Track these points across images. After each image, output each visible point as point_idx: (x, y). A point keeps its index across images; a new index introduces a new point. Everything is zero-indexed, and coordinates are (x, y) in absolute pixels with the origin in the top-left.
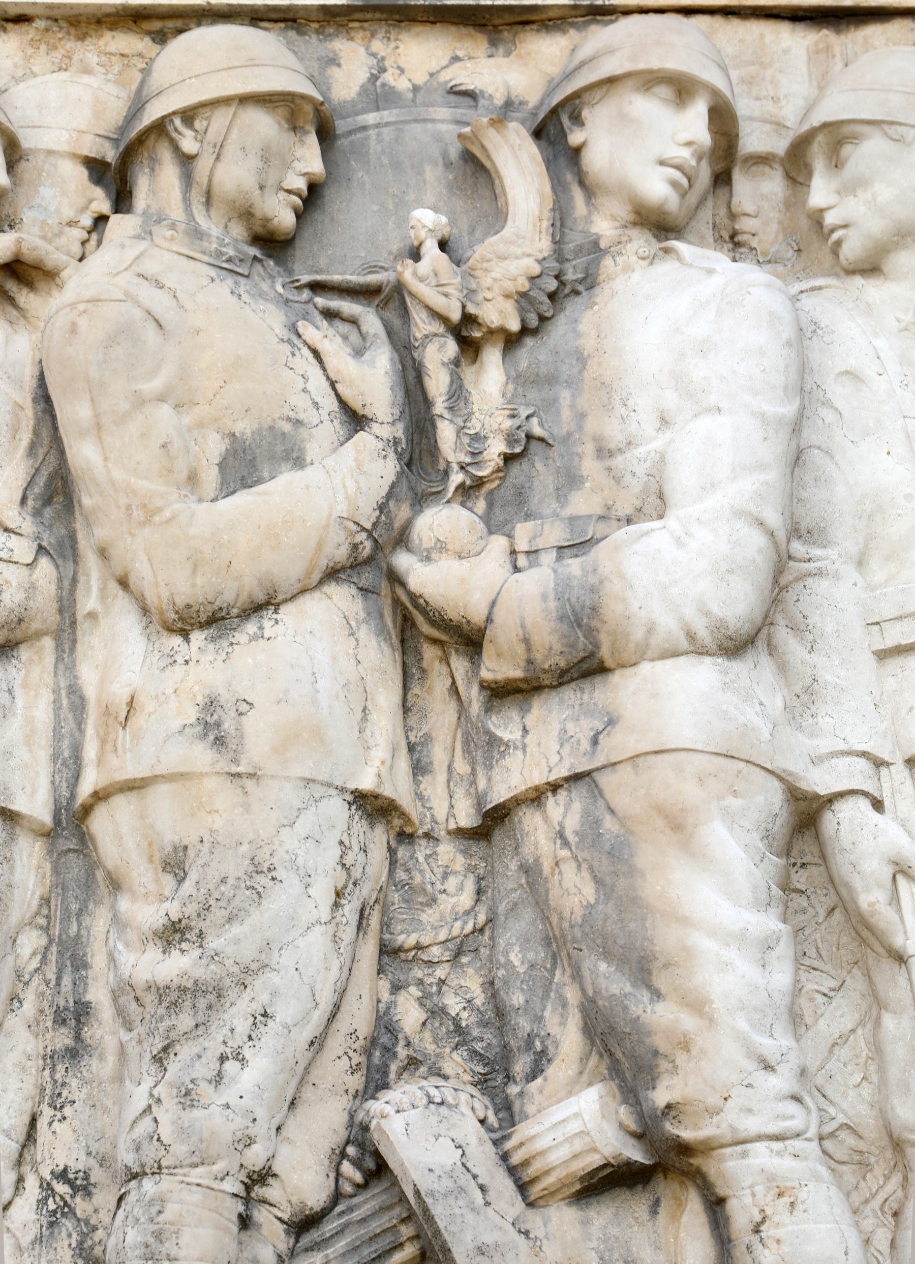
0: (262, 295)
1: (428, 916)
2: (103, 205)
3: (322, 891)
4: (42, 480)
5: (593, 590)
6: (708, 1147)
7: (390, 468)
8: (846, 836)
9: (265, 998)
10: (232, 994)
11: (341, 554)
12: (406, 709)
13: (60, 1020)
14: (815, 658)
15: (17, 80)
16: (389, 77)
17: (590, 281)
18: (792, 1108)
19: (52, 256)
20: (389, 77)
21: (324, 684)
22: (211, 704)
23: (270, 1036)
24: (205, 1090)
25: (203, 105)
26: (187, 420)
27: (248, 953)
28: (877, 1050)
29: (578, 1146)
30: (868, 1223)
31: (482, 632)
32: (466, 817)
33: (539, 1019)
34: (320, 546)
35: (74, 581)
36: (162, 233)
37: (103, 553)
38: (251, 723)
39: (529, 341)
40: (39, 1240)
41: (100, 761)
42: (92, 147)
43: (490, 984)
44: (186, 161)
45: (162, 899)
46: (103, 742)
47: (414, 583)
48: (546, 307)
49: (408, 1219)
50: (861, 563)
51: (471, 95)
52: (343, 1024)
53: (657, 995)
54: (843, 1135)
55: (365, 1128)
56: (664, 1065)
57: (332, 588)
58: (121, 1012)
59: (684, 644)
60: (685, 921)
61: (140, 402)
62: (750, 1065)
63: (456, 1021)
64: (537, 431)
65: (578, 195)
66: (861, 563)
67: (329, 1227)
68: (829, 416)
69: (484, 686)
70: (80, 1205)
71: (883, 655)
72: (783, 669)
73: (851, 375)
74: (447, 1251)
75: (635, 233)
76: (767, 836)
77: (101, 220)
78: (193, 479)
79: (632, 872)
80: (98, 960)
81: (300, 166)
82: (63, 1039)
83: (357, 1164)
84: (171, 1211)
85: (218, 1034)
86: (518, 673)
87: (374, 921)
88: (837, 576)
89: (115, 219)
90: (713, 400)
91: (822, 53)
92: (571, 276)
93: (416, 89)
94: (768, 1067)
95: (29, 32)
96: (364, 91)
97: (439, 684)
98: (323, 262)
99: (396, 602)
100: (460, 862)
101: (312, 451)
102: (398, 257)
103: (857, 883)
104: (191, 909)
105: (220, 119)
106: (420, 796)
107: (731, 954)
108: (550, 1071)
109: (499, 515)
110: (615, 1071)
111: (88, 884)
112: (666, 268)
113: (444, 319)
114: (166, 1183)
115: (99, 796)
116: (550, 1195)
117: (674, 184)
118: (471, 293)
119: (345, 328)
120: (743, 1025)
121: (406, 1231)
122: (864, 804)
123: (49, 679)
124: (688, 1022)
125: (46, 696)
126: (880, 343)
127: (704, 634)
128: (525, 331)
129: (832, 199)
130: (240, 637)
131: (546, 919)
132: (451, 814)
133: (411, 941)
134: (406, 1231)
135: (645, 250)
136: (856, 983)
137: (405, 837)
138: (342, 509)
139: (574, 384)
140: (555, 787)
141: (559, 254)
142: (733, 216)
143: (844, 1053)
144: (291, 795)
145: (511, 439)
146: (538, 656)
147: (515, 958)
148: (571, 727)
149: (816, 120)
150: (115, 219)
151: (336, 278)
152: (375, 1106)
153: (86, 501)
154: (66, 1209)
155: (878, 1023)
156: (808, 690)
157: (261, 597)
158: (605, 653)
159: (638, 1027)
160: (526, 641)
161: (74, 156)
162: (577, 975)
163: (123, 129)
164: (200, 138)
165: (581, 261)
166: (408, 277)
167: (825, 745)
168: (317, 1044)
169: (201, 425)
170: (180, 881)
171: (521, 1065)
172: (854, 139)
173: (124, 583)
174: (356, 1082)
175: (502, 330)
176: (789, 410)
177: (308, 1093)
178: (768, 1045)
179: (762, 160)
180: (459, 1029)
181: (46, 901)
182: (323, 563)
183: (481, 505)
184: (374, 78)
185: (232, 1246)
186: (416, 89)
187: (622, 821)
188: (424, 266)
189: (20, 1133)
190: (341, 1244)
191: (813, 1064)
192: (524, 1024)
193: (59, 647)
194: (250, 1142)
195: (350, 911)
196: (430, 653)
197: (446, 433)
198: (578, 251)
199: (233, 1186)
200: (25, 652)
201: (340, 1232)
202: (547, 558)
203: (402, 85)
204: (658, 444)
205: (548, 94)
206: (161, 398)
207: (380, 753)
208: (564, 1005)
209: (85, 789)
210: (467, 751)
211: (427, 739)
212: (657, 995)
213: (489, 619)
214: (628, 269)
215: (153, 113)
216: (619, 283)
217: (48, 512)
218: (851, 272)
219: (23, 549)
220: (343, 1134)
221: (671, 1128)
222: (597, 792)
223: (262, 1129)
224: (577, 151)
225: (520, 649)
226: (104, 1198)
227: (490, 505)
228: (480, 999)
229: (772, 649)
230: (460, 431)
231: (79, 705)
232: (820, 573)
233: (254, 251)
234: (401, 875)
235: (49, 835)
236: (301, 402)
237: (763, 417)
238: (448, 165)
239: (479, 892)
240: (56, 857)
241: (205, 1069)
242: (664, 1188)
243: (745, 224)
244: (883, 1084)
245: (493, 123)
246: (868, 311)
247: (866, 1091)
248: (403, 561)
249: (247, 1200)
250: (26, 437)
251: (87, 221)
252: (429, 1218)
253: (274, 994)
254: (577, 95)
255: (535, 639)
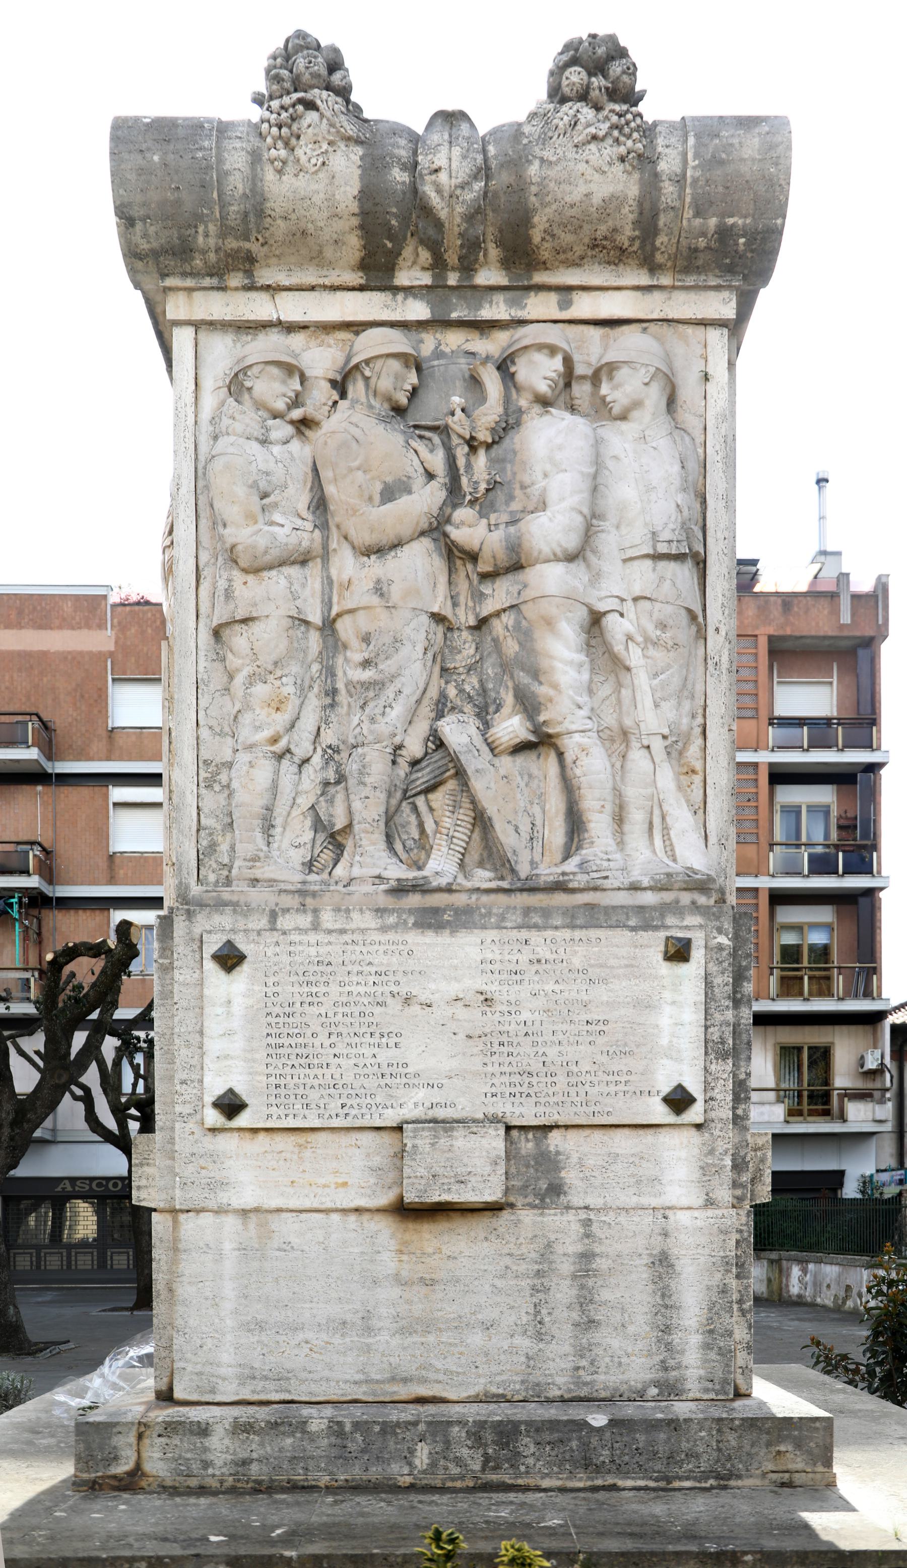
0: (395, 430)
1: (459, 657)
2: (336, 397)
3: (420, 649)
4: (315, 501)
5: (519, 538)
6: (558, 735)
7: (443, 494)
8: (610, 626)
9: (399, 686)
10: (388, 685)
11: (426, 526)
12: (450, 583)
13: (327, 694)
14: (600, 562)
15: (304, 351)
16: (442, 347)
17: (518, 423)
18: (588, 721)
19: (318, 416)
20: (442, 347)
21: (420, 574)
22: (378, 581)
23: (402, 699)
24: (379, 717)
25: (372, 358)
26: (368, 477)
27: (393, 670)
28: (619, 701)
29: (512, 735)
30: (614, 760)
31: (478, 554)
32: (472, 622)
33: (498, 693)
34: (418, 523)
35: (328, 537)
36: (358, 407)
37: (338, 527)
38: (394, 588)
39: (495, 446)
40: (322, 768)
41: (338, 603)
42: (331, 375)
43: (481, 681)
44: (367, 379)
45: (362, 651)
46: (340, 596)
47: (453, 536)
48: (502, 434)
49: (452, 761)
50: (618, 527)
51: (473, 354)
52: (428, 694)
53: (541, 683)
54: (606, 731)
55: (436, 731)
56: (543, 707)
57: (422, 539)
58: (348, 691)
59: (552, 557)
60: (551, 657)
61: (351, 470)
62: (573, 707)
63: (469, 694)
64: (498, 479)
65: (514, 391)
66: (618, 527)
67: (424, 764)
68: (607, 473)
69: (479, 574)
70: (336, 756)
71: (625, 561)
72: (588, 566)
73: (616, 458)
74: (465, 771)
75: (535, 405)
76: (581, 627)
77: (336, 403)
78: (370, 499)
79: (532, 640)
80: (340, 673)
81: (410, 381)
82: (328, 701)
83: (433, 743)
84: (368, 759)
85: (383, 698)
86: (491, 569)
87: (439, 659)
88: (609, 532)
89: (340, 402)
90: (563, 467)
91: (605, 337)
92: (511, 421)
93: (452, 352)
94: (580, 707)
95: (308, 332)
96: (433, 352)
97: (463, 574)
98: (418, 417)
99: (446, 544)
100: (470, 638)
101: (415, 488)
102: (446, 415)
103: (614, 643)
104: (372, 655)
105: (379, 363)
106: (455, 614)
107: (568, 668)
108: (502, 710)
109: (484, 511)
110: (526, 710)
111: (336, 647)
112: (547, 418)
113: (463, 438)
114: (366, 749)
115: (339, 615)
116: (502, 752)
117: (550, 386)
118: (473, 428)
119: (427, 442)
120: (571, 693)
121: (451, 765)
122: (617, 615)
123: (319, 573)
124: (551, 692)
125: (319, 580)
126: (626, 445)
127: (559, 553)
128: (494, 442)
129: (609, 392)
130: (389, 557)
131: (501, 658)
132: (467, 621)
133: (452, 666)
134: (451, 765)
135: (539, 412)
136: (612, 678)
137: (450, 629)
138: (426, 509)
139: (512, 462)
140: (504, 610)
141: (506, 413)
142: (572, 399)
143: (607, 702)
144: (408, 614)
145: (488, 483)
146: (498, 563)
147: (490, 671)
148: (511, 589)
149: (603, 362)
150: (340, 402)
151: (423, 423)
152: (439, 723)
153: (332, 508)
154: (331, 758)
155: (619, 692)
156: (598, 574)
157: (396, 542)
158: (523, 561)
159: (534, 695)
160: (494, 557)
161: (325, 379)
162: (512, 677)
163: (343, 368)
164: (372, 370)
165: (515, 416)
166: (450, 422)
167: (603, 594)
168: (419, 702)
169: (373, 479)
170: (368, 645)
171: (492, 709)
172: (617, 368)
173: (346, 538)
174: (433, 715)
175: (485, 442)
176: (592, 470)
177: (415, 719)
178: (580, 700)
179: (583, 377)
180: (469, 697)
181: (321, 653)
182: (419, 529)
183: (477, 508)
184: (437, 348)
185: (390, 770)
186: (452, 352)
187: (529, 622)
188: (456, 418)
189: (315, 733)
190: (428, 770)
191: (596, 706)
192: (493, 695)
193: (323, 562)
194: (395, 735)
195: (430, 655)
196: (459, 563)
197: (464, 480)
198: (514, 412)
199: (389, 750)
200: (311, 564)
201: (428, 766)
202: (502, 527)
203: (447, 350)
204: (543, 484)
205: (502, 353)
206: (358, 469)
207: (440, 599)
208: (507, 687)
209: (334, 613)
210: (472, 598)
211: (458, 594)
212: (541, 683)
213: (480, 549)
214: (532, 418)
215: (354, 361)
216: (529, 424)
217: (318, 512)
218: (616, 419)
219: (309, 526)
220: (428, 733)
221: (545, 729)
222: (520, 612)
223: (399, 731)
224: (513, 374)
225: (492, 560)
226: (344, 755)
227: (481, 507)
228: (477, 686)
229: (585, 559)
230: (469, 480)
231: (330, 582)
232: (602, 531)
233: (392, 413)
234: (448, 643)
235: (321, 629)
236: (410, 470)
237: (582, 473)
238: (465, 380)
239: (477, 648)
240: (324, 638)
241: (379, 710)
242: (542, 749)
243: (576, 402)
244: (621, 712)
245: (482, 364)
246: (622, 433)
247: (615, 715)
248: (449, 529)
249: (395, 755)
250: (309, 485)
251: (330, 403)
252: (459, 760)
253: (403, 684)
254: (513, 353)
255: (498, 556)
